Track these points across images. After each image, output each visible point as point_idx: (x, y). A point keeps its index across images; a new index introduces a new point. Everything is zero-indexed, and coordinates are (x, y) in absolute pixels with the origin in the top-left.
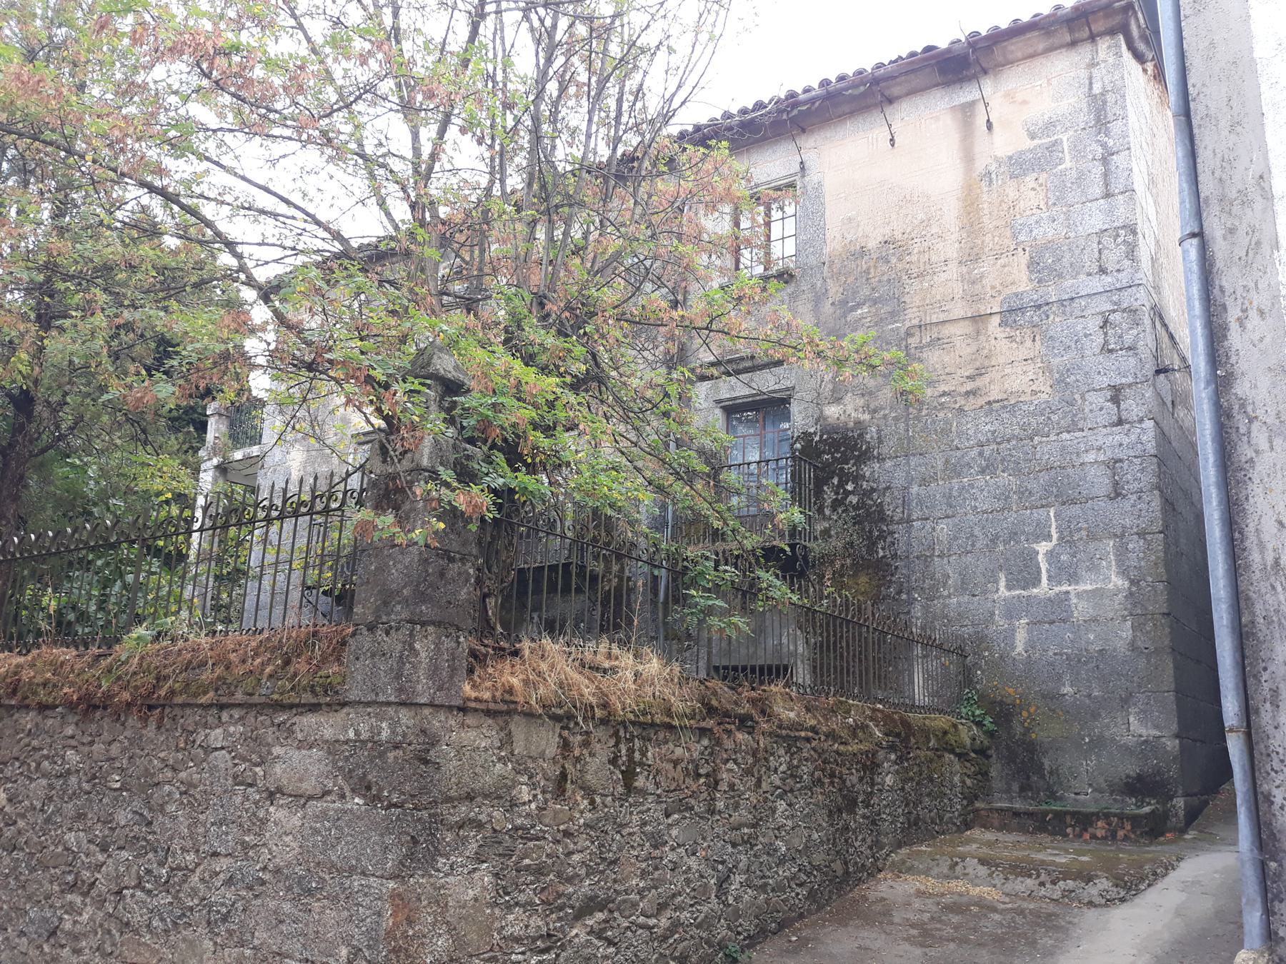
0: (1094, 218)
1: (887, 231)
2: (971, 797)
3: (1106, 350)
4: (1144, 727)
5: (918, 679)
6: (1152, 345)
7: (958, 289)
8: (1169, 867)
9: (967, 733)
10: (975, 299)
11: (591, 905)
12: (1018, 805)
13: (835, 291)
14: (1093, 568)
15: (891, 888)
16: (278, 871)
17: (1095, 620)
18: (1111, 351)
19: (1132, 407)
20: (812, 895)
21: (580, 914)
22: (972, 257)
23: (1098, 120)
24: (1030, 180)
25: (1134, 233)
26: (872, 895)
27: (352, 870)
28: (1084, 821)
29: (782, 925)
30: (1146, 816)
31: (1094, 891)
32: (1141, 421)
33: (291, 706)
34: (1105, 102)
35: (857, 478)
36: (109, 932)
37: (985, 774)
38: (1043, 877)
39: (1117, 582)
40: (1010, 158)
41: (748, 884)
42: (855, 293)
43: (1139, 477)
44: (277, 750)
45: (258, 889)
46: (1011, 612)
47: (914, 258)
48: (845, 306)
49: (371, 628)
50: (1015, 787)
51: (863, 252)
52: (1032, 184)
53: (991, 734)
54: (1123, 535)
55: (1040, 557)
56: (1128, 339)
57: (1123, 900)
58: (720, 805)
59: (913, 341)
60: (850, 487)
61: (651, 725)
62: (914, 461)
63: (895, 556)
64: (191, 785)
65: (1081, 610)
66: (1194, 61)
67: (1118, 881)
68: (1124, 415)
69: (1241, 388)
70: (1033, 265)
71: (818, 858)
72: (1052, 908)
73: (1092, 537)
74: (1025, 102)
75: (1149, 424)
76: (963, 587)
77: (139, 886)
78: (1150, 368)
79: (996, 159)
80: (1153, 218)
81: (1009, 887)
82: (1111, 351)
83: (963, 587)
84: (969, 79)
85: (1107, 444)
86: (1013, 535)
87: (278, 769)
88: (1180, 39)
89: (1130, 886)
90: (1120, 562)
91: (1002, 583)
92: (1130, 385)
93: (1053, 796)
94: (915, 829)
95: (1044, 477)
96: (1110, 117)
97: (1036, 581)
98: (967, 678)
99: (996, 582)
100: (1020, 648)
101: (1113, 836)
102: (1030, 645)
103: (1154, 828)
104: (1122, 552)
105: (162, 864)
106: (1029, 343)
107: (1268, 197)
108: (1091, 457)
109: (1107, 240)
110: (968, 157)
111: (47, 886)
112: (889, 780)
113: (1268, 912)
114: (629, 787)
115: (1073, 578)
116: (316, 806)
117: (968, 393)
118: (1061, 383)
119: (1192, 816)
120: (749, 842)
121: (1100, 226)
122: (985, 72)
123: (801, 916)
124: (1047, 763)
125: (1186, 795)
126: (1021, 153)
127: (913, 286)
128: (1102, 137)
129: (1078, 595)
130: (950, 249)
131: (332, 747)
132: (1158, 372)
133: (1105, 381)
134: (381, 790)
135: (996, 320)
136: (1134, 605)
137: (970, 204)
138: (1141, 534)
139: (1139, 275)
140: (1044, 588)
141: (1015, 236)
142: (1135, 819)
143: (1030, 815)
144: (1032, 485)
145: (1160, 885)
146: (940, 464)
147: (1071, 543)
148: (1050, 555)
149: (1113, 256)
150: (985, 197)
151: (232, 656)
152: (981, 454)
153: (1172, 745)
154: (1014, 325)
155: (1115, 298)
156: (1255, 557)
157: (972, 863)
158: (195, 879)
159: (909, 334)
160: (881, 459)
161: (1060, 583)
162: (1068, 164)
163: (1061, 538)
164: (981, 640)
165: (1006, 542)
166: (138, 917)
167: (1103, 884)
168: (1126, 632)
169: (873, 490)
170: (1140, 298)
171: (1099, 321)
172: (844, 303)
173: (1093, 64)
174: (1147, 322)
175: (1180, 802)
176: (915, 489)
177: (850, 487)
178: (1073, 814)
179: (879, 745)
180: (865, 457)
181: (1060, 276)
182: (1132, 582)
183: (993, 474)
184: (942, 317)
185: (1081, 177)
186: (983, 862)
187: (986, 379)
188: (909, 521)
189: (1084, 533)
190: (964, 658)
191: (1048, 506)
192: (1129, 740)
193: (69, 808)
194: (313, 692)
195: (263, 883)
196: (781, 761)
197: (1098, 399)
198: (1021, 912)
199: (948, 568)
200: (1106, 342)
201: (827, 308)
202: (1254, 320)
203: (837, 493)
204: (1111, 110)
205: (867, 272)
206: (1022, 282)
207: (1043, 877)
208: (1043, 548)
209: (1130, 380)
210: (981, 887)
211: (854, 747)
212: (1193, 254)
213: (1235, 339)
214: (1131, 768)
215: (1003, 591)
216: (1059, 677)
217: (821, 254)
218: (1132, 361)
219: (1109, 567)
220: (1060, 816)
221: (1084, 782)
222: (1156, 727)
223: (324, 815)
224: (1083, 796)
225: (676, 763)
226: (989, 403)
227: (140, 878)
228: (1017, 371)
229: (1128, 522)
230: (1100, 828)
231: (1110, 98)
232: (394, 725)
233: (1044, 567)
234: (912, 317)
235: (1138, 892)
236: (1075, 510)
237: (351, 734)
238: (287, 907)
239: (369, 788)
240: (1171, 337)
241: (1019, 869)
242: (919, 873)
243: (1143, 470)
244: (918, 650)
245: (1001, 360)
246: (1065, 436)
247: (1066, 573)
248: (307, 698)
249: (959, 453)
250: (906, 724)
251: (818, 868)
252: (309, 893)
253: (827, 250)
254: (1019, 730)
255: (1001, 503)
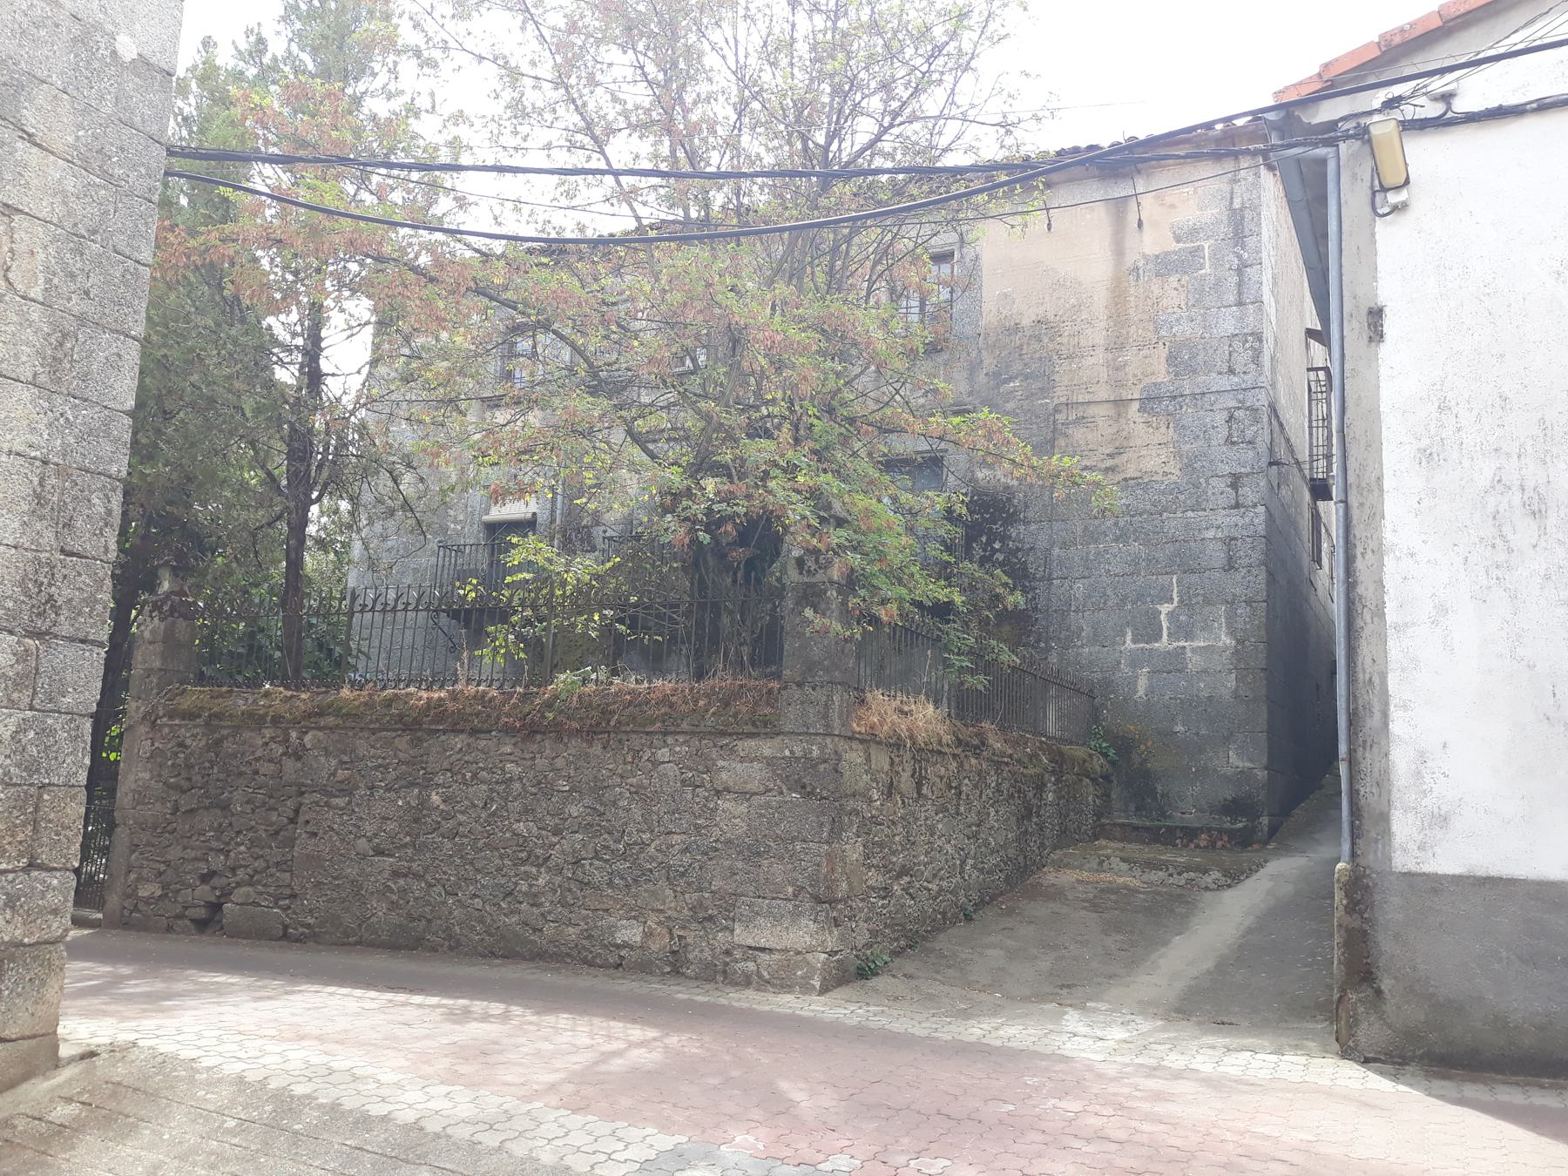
0: (1227, 324)
1: (1041, 311)
2: (1099, 815)
3: (1229, 441)
4: (1241, 761)
5: (1051, 715)
6: (1268, 439)
7: (1104, 374)
8: (1260, 866)
9: (1098, 763)
10: (1118, 384)
11: (904, 871)
12: (1135, 821)
13: (989, 361)
14: (1206, 628)
15: (1051, 877)
16: (729, 842)
17: (1205, 671)
18: (1233, 443)
19: (1249, 493)
20: (1007, 880)
21: (899, 876)
22: (1117, 346)
23: (1236, 234)
24: (1173, 279)
25: (1261, 341)
26: (1045, 883)
27: (793, 839)
28: (1190, 834)
29: (992, 899)
30: (1240, 830)
31: (1209, 880)
32: (1255, 506)
33: (730, 735)
34: (1243, 218)
35: (1004, 538)
36: (570, 890)
37: (1108, 796)
38: (1171, 870)
39: (1226, 640)
40: (1157, 257)
41: (974, 867)
42: (1008, 366)
43: (1249, 554)
44: (720, 763)
45: (712, 854)
46: (1135, 663)
47: (1065, 340)
48: (998, 378)
49: (800, 685)
50: (1132, 807)
51: (1017, 328)
52: (1175, 284)
53: (1113, 763)
54: (1233, 603)
55: (1162, 617)
56: (1249, 434)
57: (1229, 886)
58: (962, 809)
59: (1061, 417)
60: (997, 546)
61: (924, 753)
62: (1056, 526)
63: (1035, 609)
64: (641, 786)
65: (1194, 662)
66: (1349, 403)
67: (1226, 873)
68: (1241, 500)
69: (1360, 590)
70: (1172, 359)
71: (1012, 852)
72: (1179, 891)
73: (1208, 602)
74: (1172, 206)
75: (1261, 509)
76: (1095, 638)
77: (597, 856)
78: (1264, 461)
79: (1144, 256)
80: (1273, 320)
81: (1146, 877)
82: (1233, 443)
83: (1095, 638)
84: (1125, 176)
85: (1224, 523)
86: (1140, 596)
87: (724, 775)
88: (1343, 355)
89: (1234, 877)
90: (1229, 625)
91: (1129, 637)
92: (1247, 475)
93: (1163, 815)
94: (1066, 837)
95: (1170, 548)
96: (1247, 232)
97: (1157, 637)
98: (1096, 719)
99: (1124, 635)
100: (1141, 693)
101: (1214, 847)
102: (1150, 690)
103: (1244, 840)
104: (1231, 617)
105: (617, 841)
106: (1163, 429)
107: (1381, 490)
108: (1210, 534)
109: (1237, 344)
110: (1119, 251)
111: (498, 861)
112: (1051, 797)
113: (1353, 844)
114: (919, 793)
115: (1189, 636)
116: (756, 800)
117: (1107, 469)
118: (1189, 467)
119: (1273, 831)
120: (975, 836)
121: (1231, 330)
122: (1139, 172)
123: (1002, 894)
124: (1159, 788)
125: (1270, 815)
126: (1167, 253)
127: (1062, 367)
128: (1238, 249)
129: (1193, 650)
130: (1097, 335)
131: (770, 762)
132: (1271, 464)
133: (1227, 469)
134: (814, 788)
135: (1135, 406)
136: (1239, 661)
137: (1118, 295)
138: (1249, 602)
139: (1262, 378)
140: (1164, 643)
141: (1157, 331)
142: (1232, 834)
143: (1147, 829)
144: (1160, 555)
145: (1255, 877)
146: (1079, 530)
147: (1190, 606)
148: (1170, 615)
149: (1242, 358)
150: (1132, 291)
151: (674, 699)
152: (1116, 524)
153: (1262, 775)
154: (1151, 412)
155: (1241, 397)
156: (1361, 676)
157: (1115, 861)
158: (652, 849)
159: (1056, 410)
160: (1027, 522)
161: (1178, 640)
162: (1207, 270)
163: (1181, 601)
164: (1107, 684)
165: (1134, 603)
166: (598, 877)
167: (1216, 875)
168: (1231, 682)
169: (1018, 550)
170: (1262, 400)
171: (1225, 415)
172: (997, 375)
173: (1235, 181)
174: (1265, 419)
175: (1265, 820)
176: (1056, 551)
177: (997, 546)
178: (1182, 828)
179: (1045, 769)
180: (1012, 519)
181: (1194, 372)
182: (1238, 641)
183: (1126, 543)
184: (1088, 398)
185: (1218, 283)
186: (1123, 860)
187: (1125, 457)
188: (1050, 579)
189: (1200, 598)
190: (1092, 698)
191: (1172, 573)
192: (1229, 771)
193: (516, 805)
194: (754, 724)
195: (717, 850)
196: (992, 780)
197: (1220, 485)
198: (1159, 893)
199: (1083, 622)
200: (1230, 435)
201: (981, 378)
202: (1369, 555)
203: (985, 550)
204: (1248, 226)
205: (1021, 347)
206: (1161, 373)
207: (1171, 870)
208: (1165, 609)
209: (1248, 470)
210: (1126, 878)
211: (1031, 771)
212: (1341, 513)
213: (1360, 564)
214: (1228, 793)
215: (1129, 644)
216: (1173, 720)
217: (977, 326)
218: (1251, 453)
219: (1220, 628)
220: (1171, 830)
221: (1190, 803)
222: (1251, 761)
223: (768, 805)
224: (1190, 815)
225: (941, 778)
226: (1125, 480)
227: (596, 852)
228: (1153, 454)
229: (1238, 591)
230: (1203, 839)
231: (1248, 214)
232: (822, 748)
233: (1165, 625)
234: (1060, 395)
235: (1240, 881)
236: (1194, 578)
237: (787, 753)
238: (740, 865)
239: (804, 787)
240: (1281, 425)
241: (1151, 865)
242: (1074, 868)
243: (1253, 548)
244: (1052, 692)
245: (1139, 442)
246: (1190, 514)
247: (1183, 630)
248: (748, 728)
249: (1097, 522)
250: (1061, 754)
251: (1010, 859)
252: (759, 854)
253: (983, 323)
254: (1136, 759)
255: (1132, 569)
